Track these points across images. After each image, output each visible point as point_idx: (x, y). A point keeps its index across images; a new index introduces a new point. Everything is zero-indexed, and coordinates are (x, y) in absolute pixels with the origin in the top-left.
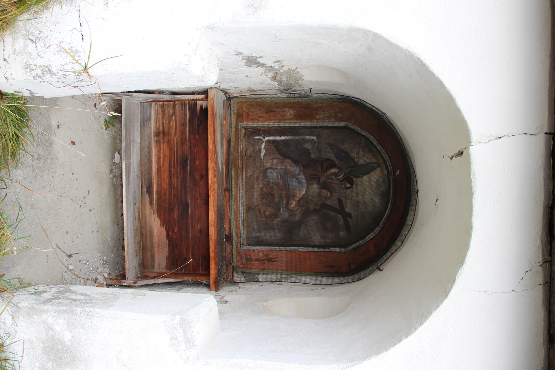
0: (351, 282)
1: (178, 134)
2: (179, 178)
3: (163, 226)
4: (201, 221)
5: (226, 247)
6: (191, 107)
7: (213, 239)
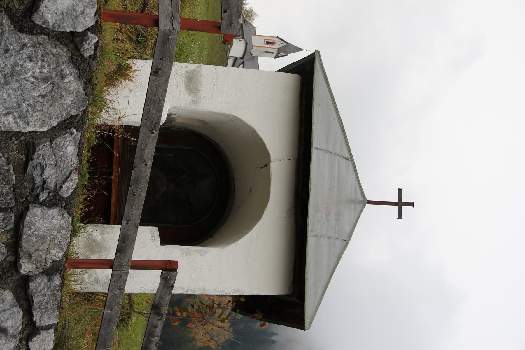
7: (113, 214)
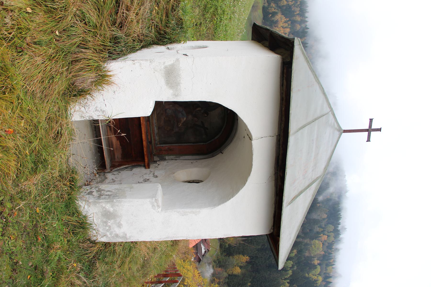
3: (118, 140)
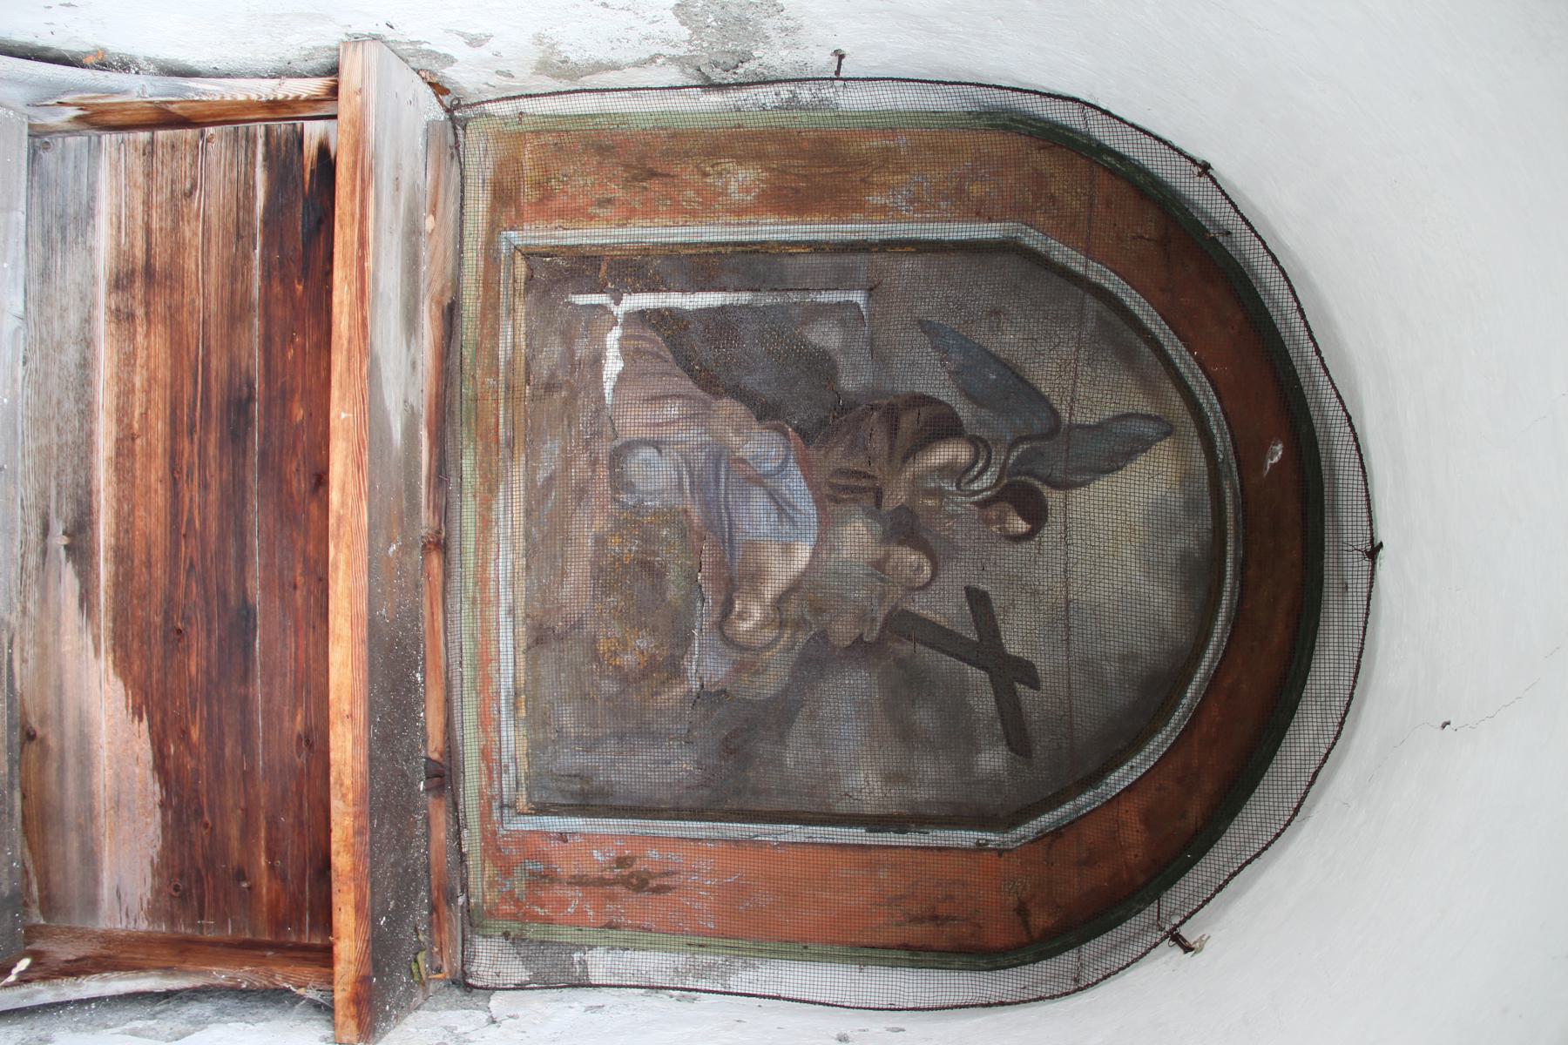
0: (1035, 1000)
1: (213, 279)
2: (214, 485)
3: (137, 712)
4: (308, 692)
5: (427, 820)
6: (279, 149)
7: (348, 782)
